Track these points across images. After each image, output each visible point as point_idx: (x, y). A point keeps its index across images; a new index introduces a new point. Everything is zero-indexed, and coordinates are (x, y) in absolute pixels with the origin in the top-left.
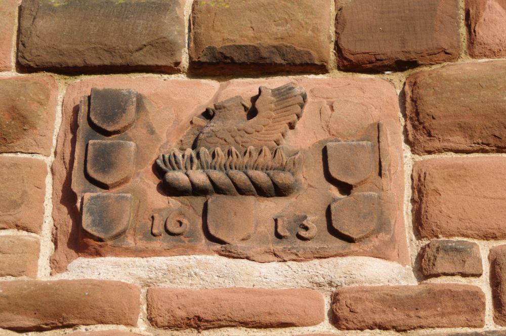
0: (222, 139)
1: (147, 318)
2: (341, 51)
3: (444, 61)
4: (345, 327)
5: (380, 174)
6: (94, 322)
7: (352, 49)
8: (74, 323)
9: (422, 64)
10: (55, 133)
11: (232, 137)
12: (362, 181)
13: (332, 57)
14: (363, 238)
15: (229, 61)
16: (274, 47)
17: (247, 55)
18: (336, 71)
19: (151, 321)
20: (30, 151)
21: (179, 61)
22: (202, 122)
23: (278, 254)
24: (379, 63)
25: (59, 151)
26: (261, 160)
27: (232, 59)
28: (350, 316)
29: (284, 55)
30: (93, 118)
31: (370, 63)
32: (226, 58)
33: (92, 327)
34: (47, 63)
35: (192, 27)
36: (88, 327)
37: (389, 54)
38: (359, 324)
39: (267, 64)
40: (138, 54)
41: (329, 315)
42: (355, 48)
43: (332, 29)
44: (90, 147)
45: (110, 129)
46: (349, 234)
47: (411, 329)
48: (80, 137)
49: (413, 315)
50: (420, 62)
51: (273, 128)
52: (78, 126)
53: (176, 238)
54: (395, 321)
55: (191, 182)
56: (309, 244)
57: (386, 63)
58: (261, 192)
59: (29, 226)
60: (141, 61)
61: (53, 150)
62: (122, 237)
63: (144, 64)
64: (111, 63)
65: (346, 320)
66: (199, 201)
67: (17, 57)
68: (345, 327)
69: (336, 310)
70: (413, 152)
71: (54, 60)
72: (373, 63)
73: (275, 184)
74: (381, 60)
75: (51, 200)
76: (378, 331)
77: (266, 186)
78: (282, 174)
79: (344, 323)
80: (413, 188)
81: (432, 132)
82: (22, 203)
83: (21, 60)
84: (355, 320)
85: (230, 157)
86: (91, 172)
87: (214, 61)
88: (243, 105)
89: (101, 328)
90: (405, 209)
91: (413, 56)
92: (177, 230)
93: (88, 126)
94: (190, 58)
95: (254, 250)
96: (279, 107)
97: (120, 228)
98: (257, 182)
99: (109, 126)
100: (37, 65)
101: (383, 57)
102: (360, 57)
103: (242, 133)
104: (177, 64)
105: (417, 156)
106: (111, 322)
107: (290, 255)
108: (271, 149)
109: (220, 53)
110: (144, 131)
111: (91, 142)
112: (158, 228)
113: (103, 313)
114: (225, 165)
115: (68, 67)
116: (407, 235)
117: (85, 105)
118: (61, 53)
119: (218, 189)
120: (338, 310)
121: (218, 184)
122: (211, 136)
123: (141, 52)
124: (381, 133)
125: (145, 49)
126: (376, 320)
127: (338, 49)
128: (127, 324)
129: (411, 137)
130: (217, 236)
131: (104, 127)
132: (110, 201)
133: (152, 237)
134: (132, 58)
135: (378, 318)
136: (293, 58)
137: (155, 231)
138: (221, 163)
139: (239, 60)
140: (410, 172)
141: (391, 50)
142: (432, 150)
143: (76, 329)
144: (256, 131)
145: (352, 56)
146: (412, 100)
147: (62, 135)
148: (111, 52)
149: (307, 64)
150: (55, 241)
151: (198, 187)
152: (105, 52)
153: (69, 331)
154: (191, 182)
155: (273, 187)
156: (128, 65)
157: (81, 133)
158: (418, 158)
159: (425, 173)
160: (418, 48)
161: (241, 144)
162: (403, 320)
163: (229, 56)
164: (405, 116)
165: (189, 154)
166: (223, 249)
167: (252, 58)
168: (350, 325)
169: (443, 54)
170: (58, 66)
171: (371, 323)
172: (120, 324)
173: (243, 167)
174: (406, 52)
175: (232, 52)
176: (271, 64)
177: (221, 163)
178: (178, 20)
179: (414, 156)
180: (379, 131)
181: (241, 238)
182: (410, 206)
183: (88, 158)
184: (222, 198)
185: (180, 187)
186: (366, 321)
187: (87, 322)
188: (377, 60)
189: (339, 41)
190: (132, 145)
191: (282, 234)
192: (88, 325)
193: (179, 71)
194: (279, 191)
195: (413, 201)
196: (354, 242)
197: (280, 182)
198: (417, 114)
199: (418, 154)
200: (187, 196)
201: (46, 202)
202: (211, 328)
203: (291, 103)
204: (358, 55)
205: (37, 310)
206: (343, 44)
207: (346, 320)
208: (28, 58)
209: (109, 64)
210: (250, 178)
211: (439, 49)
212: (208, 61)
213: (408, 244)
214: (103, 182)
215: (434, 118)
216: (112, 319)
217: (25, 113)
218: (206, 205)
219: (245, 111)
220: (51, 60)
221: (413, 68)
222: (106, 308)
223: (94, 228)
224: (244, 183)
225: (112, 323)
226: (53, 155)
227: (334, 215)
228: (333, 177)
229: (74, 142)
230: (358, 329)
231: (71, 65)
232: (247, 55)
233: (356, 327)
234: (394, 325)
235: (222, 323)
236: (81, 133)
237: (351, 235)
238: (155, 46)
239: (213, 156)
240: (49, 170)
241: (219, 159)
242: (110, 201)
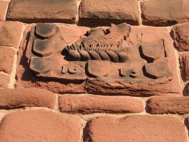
0: (94, 40)
1: (59, 108)
2: (144, 17)
3: (187, 22)
4: (154, 113)
5: (166, 56)
6: (34, 105)
7: (149, 15)
8: (24, 105)
9: (179, 23)
10: (20, 41)
11: (99, 40)
12: (158, 57)
13: (140, 20)
14: (161, 77)
15: (96, 18)
16: (116, 12)
17: (104, 15)
18: (142, 25)
19: (60, 109)
20: (9, 45)
21: (75, 17)
22: (85, 37)
23: (121, 82)
24: (161, 21)
25: (21, 47)
26: (112, 48)
27: (98, 17)
28: (157, 107)
29: (120, 16)
30: (37, 32)
31: (157, 21)
32: (95, 16)
33: (32, 108)
34: (19, 17)
35: (80, 7)
36: (30, 108)
37: (165, 18)
38: (161, 111)
39: (113, 19)
40: (57, 15)
41: (145, 109)
42: (151, 15)
43: (140, 10)
44: (35, 42)
45: (44, 36)
46: (154, 75)
47: (186, 113)
48: (31, 39)
49: (186, 107)
50: (178, 22)
51: (117, 38)
52: (30, 36)
53: (73, 75)
54: (178, 109)
55: (81, 54)
56: (136, 79)
57: (164, 21)
58: (112, 59)
59: (6, 70)
60: (59, 17)
61: (18, 47)
62: (48, 73)
63: (60, 18)
64: (46, 17)
65: (155, 109)
66: (84, 63)
67: (7, 16)
68: (154, 113)
69: (150, 106)
70: (179, 51)
71: (22, 16)
72: (158, 21)
73: (119, 56)
74: (162, 20)
75: (16, 64)
76: (170, 114)
77: (115, 56)
78: (122, 52)
79: (154, 110)
80: (180, 63)
81: (187, 42)
82: (3, 60)
83: (8, 17)
84: (159, 109)
85: (98, 46)
86: (35, 50)
87: (90, 18)
88: (103, 30)
89: (36, 108)
90: (177, 70)
91: (175, 19)
92: (74, 71)
93: (35, 36)
94: (79, 17)
95: (110, 81)
96: (119, 31)
97: (47, 69)
98: (111, 55)
99: (44, 35)
100: (14, 18)
101: (162, 19)
102: (153, 19)
103: (103, 39)
104: (74, 19)
105: (181, 52)
106: (42, 106)
107: (127, 83)
108: (116, 45)
109: (93, 14)
110: (60, 39)
111: (35, 40)
112: (65, 71)
113: (38, 101)
114: (96, 49)
115: (27, 19)
116: (179, 80)
117: (33, 29)
118: (25, 14)
119: (93, 58)
120: (151, 105)
121: (93, 55)
122: (89, 39)
123: (59, 14)
124: (165, 43)
125: (60, 13)
126: (169, 109)
127: (143, 16)
128: (49, 108)
129: (177, 45)
130: (93, 74)
131: (42, 35)
132: (43, 60)
133: (62, 74)
134: (55, 16)
135: (170, 108)
136: (124, 17)
137: (63, 71)
138: (94, 48)
139: (101, 17)
140: (178, 58)
141: (165, 17)
142: (187, 49)
143: (24, 109)
144: (109, 38)
145: (149, 18)
146: (176, 33)
147: (23, 41)
148: (46, 14)
149: (130, 20)
150: (16, 78)
151: (83, 57)
152: (43, 14)
153: (21, 110)
154: (81, 54)
155: (118, 57)
156: (53, 19)
157: (31, 38)
158: (181, 53)
159: (185, 57)
160: (177, 16)
161: (103, 43)
162: (182, 109)
163: (96, 15)
164: (173, 39)
165: (79, 45)
166: (95, 79)
167: (106, 17)
168: (157, 112)
169: (187, 19)
170: (23, 18)
171: (167, 110)
172: (46, 107)
173: (104, 50)
174: (172, 17)
175: (98, 14)
176: (115, 19)
177: (94, 48)
178: (75, 5)
179: (179, 52)
180: (163, 42)
181: (104, 75)
182: (180, 70)
183: (34, 45)
184: (94, 61)
185: (75, 56)
186: (165, 109)
187: (31, 105)
188: (160, 20)
189: (143, 13)
190: (54, 42)
191: (123, 74)
192: (30, 107)
193: (74, 23)
194: (121, 59)
195: (181, 67)
196: (157, 79)
197: (121, 55)
198: (179, 36)
199: (181, 51)
200: (78, 61)
201: (14, 64)
202: (89, 113)
203: (124, 29)
204: (152, 18)
205: (7, 99)
206: (145, 13)
207: (155, 109)
208: (11, 16)
209: (45, 18)
210: (107, 53)
211: (185, 17)
212: (87, 17)
213: (180, 83)
214: (40, 53)
215: (187, 37)
216: (42, 104)
217: (7, 30)
218: (87, 65)
219: (104, 33)
220: (20, 16)
221: (174, 24)
222: (39, 99)
223: (35, 69)
224: (105, 55)
225: (42, 106)
226: (18, 48)
227: (147, 68)
228: (145, 56)
229: (27, 43)
230: (160, 113)
231: (28, 18)
232: (104, 15)
233: (160, 112)
234: (178, 111)
235: (95, 110)
236: (31, 38)
237: (155, 75)
238: (65, 13)
239: (90, 46)
240: (16, 53)
241: (93, 47)
242: (43, 60)
